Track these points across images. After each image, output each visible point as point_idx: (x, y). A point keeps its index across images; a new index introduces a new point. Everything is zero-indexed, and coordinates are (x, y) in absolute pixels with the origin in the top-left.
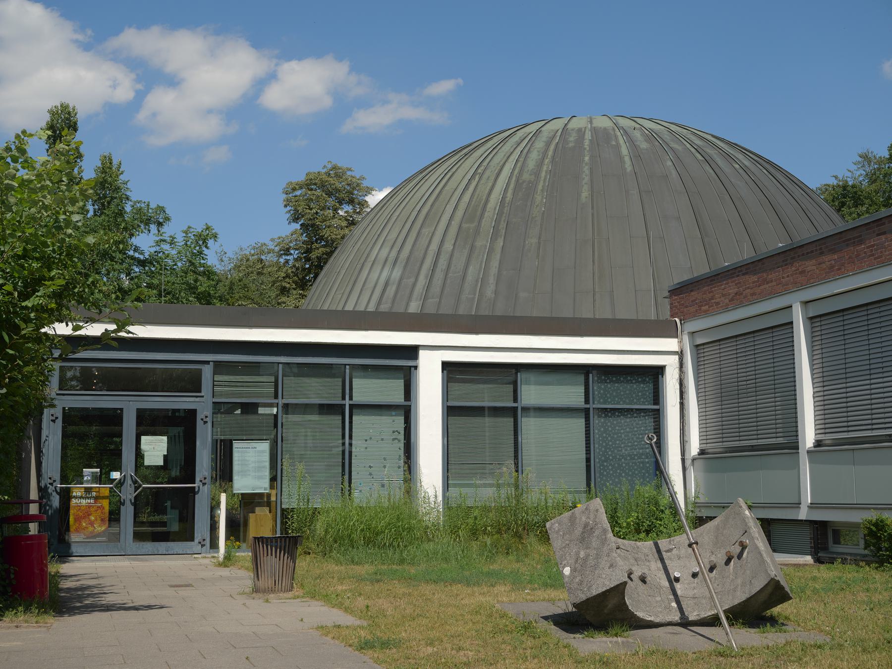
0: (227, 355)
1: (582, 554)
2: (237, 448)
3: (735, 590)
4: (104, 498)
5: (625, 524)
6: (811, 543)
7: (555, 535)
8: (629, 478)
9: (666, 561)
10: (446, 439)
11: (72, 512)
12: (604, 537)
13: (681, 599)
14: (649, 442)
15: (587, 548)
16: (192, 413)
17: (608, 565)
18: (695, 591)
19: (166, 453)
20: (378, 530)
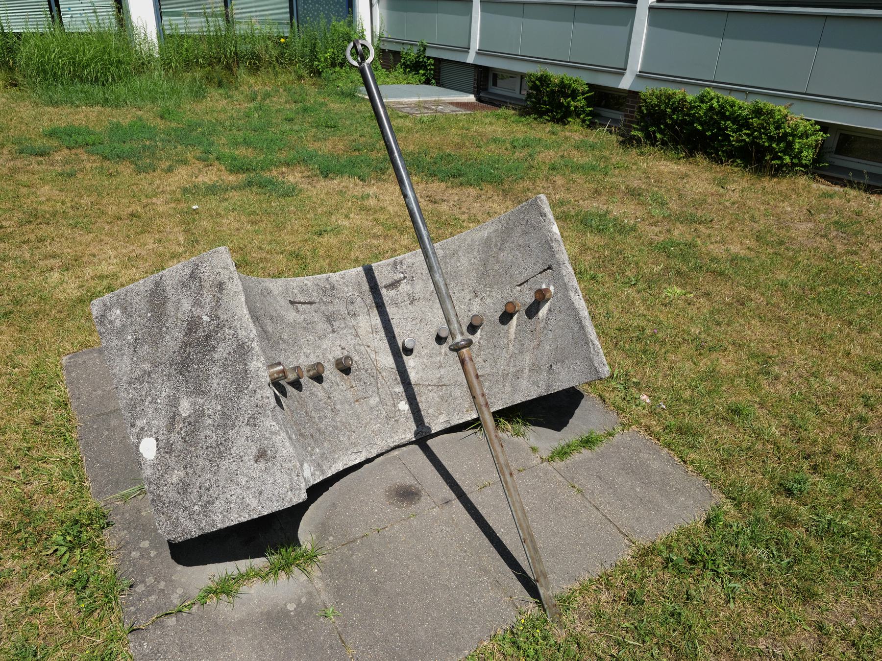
1: (185, 407)
3: (517, 376)
5: (323, 59)
7: (115, 343)
8: (326, 12)
9: (388, 310)
12: (240, 367)
13: (416, 389)
14: (355, 64)
15: (199, 391)
17: (254, 451)
18: (443, 371)
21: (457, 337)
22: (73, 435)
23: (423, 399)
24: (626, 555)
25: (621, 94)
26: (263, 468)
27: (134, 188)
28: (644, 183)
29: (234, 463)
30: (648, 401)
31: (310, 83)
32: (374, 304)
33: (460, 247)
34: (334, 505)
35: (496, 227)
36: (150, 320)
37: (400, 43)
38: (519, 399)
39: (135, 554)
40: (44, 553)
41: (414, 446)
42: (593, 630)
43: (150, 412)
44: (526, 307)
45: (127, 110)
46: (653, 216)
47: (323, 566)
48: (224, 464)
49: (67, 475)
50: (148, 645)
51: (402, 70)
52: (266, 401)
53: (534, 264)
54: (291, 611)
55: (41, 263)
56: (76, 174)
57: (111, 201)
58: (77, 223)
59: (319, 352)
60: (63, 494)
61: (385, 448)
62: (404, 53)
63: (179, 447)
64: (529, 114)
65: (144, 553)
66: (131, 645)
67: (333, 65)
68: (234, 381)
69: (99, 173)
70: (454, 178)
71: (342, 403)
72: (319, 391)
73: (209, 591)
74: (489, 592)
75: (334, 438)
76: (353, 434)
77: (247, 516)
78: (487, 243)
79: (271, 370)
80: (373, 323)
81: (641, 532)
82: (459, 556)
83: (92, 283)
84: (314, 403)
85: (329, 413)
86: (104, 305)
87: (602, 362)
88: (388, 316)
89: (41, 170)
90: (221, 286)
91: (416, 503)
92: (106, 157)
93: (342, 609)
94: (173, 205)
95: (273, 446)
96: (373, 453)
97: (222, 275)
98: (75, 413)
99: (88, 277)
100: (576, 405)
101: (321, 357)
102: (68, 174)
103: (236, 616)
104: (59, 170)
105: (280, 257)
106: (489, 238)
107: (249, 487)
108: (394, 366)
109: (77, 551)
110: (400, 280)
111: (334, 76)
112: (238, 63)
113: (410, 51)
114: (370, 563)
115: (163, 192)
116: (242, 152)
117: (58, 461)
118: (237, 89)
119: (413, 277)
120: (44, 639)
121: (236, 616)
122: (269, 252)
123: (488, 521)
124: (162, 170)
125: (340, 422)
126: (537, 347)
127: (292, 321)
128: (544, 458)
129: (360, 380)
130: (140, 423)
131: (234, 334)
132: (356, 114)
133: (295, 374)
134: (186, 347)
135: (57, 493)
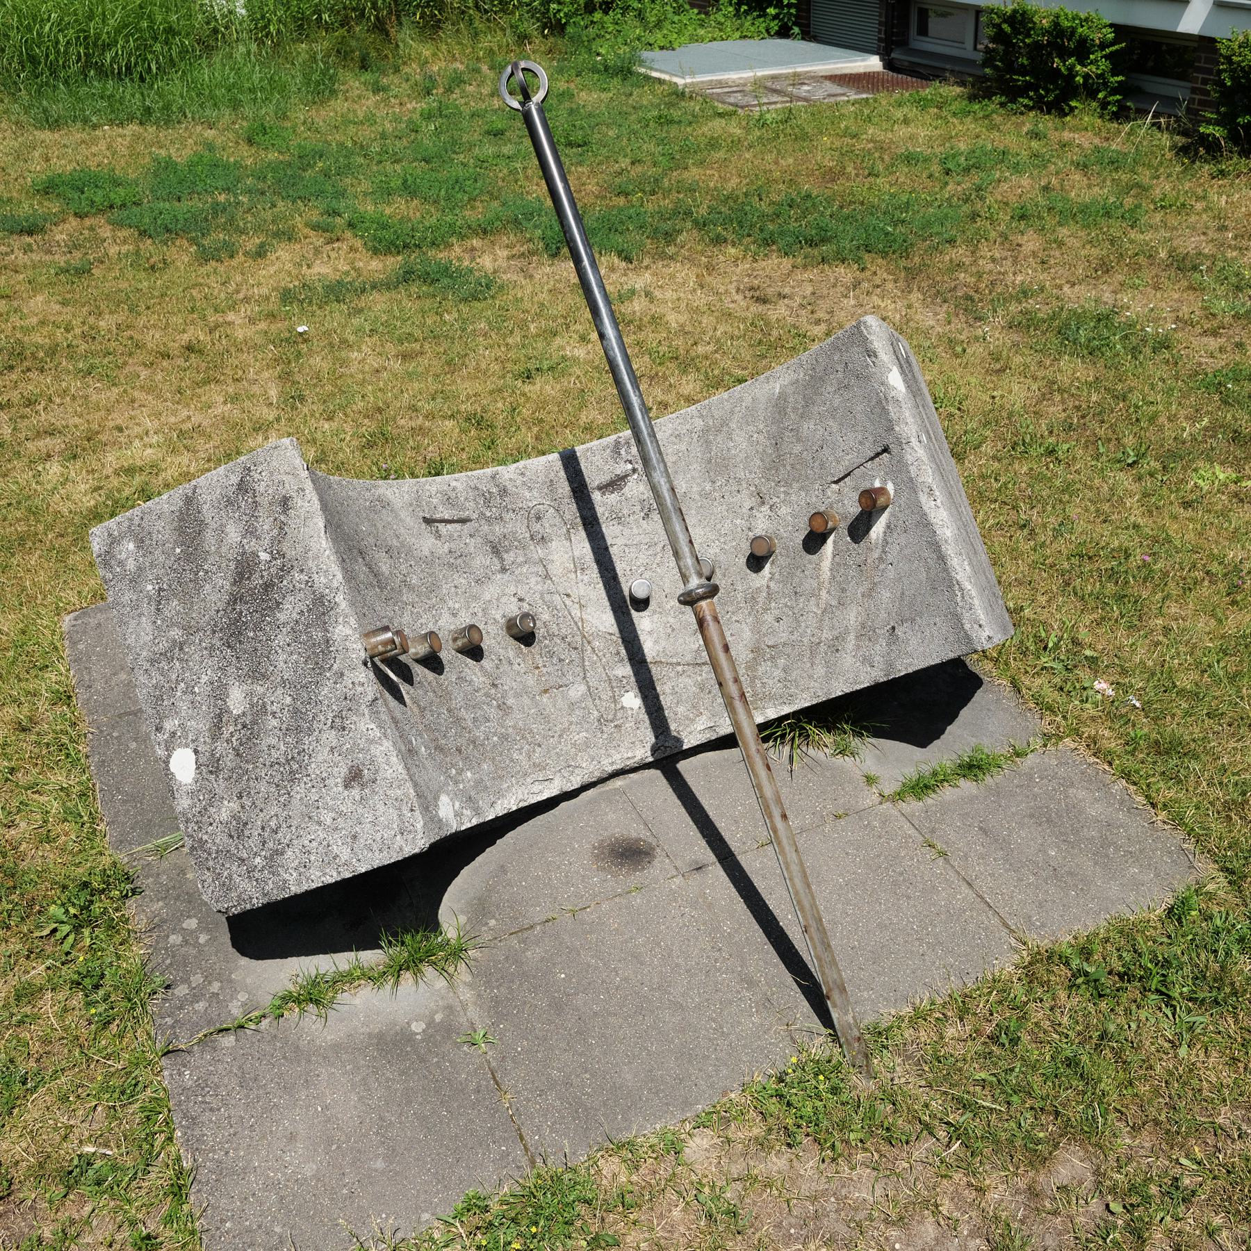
1: (237, 700)
6: (880, 32)
7: (127, 597)
9: (604, 529)
12: (318, 635)
13: (654, 670)
15: (256, 675)
17: (344, 770)
20: (104, 41)
21: (690, 580)
22: (81, 748)
24: (1006, 965)
25: (1187, 43)
26: (358, 798)
27: (194, 292)
28: (1212, 241)
29: (314, 790)
30: (1110, 692)
31: (543, 49)
32: (579, 520)
33: (732, 412)
34: (503, 869)
36: (179, 559)
38: (839, 689)
39: (175, 939)
40: (37, 934)
41: (652, 771)
42: (923, 1083)
43: (183, 706)
44: (849, 521)
45: (186, 128)
46: (1214, 315)
47: (475, 966)
48: (299, 790)
49: (71, 813)
50: (191, 1075)
51: (731, 9)
52: (360, 689)
54: (417, 1034)
55: (29, 445)
56: (91, 269)
57: (152, 322)
58: (92, 367)
59: (476, 607)
60: (66, 843)
61: (597, 774)
63: (229, 764)
64: (988, 95)
65: (189, 938)
66: (166, 1073)
68: (309, 656)
69: (131, 265)
70: (811, 246)
71: (517, 695)
72: (475, 674)
73: (287, 998)
75: (501, 755)
76: (538, 750)
77: (335, 874)
78: (780, 405)
79: (373, 640)
80: (577, 554)
81: (1043, 925)
83: (115, 482)
84: (466, 695)
85: (493, 713)
86: (110, 535)
88: (605, 541)
89: (29, 263)
90: (285, 504)
91: (643, 868)
92: (145, 231)
93: (500, 1034)
94: (263, 325)
95: (372, 762)
96: (574, 783)
97: (287, 485)
98: (84, 712)
99: (109, 471)
100: (965, 699)
101: (480, 614)
102: (76, 269)
103: (328, 1038)
104: (61, 260)
105: (449, 424)
106: (783, 396)
107: (336, 829)
108: (614, 629)
109: (86, 932)
110: (626, 476)
111: (592, 31)
112: (398, 17)
115: (247, 300)
116: (400, 209)
117: (56, 790)
118: (397, 70)
120: (38, 1061)
121: (328, 1038)
122: (430, 416)
123: (767, 902)
124: (246, 254)
125: (514, 727)
126: (869, 594)
127: (427, 553)
128: (886, 795)
129: (551, 654)
130: (169, 725)
131: (308, 582)
132: (630, 114)
133: (427, 645)
134: (235, 602)
135: (55, 842)
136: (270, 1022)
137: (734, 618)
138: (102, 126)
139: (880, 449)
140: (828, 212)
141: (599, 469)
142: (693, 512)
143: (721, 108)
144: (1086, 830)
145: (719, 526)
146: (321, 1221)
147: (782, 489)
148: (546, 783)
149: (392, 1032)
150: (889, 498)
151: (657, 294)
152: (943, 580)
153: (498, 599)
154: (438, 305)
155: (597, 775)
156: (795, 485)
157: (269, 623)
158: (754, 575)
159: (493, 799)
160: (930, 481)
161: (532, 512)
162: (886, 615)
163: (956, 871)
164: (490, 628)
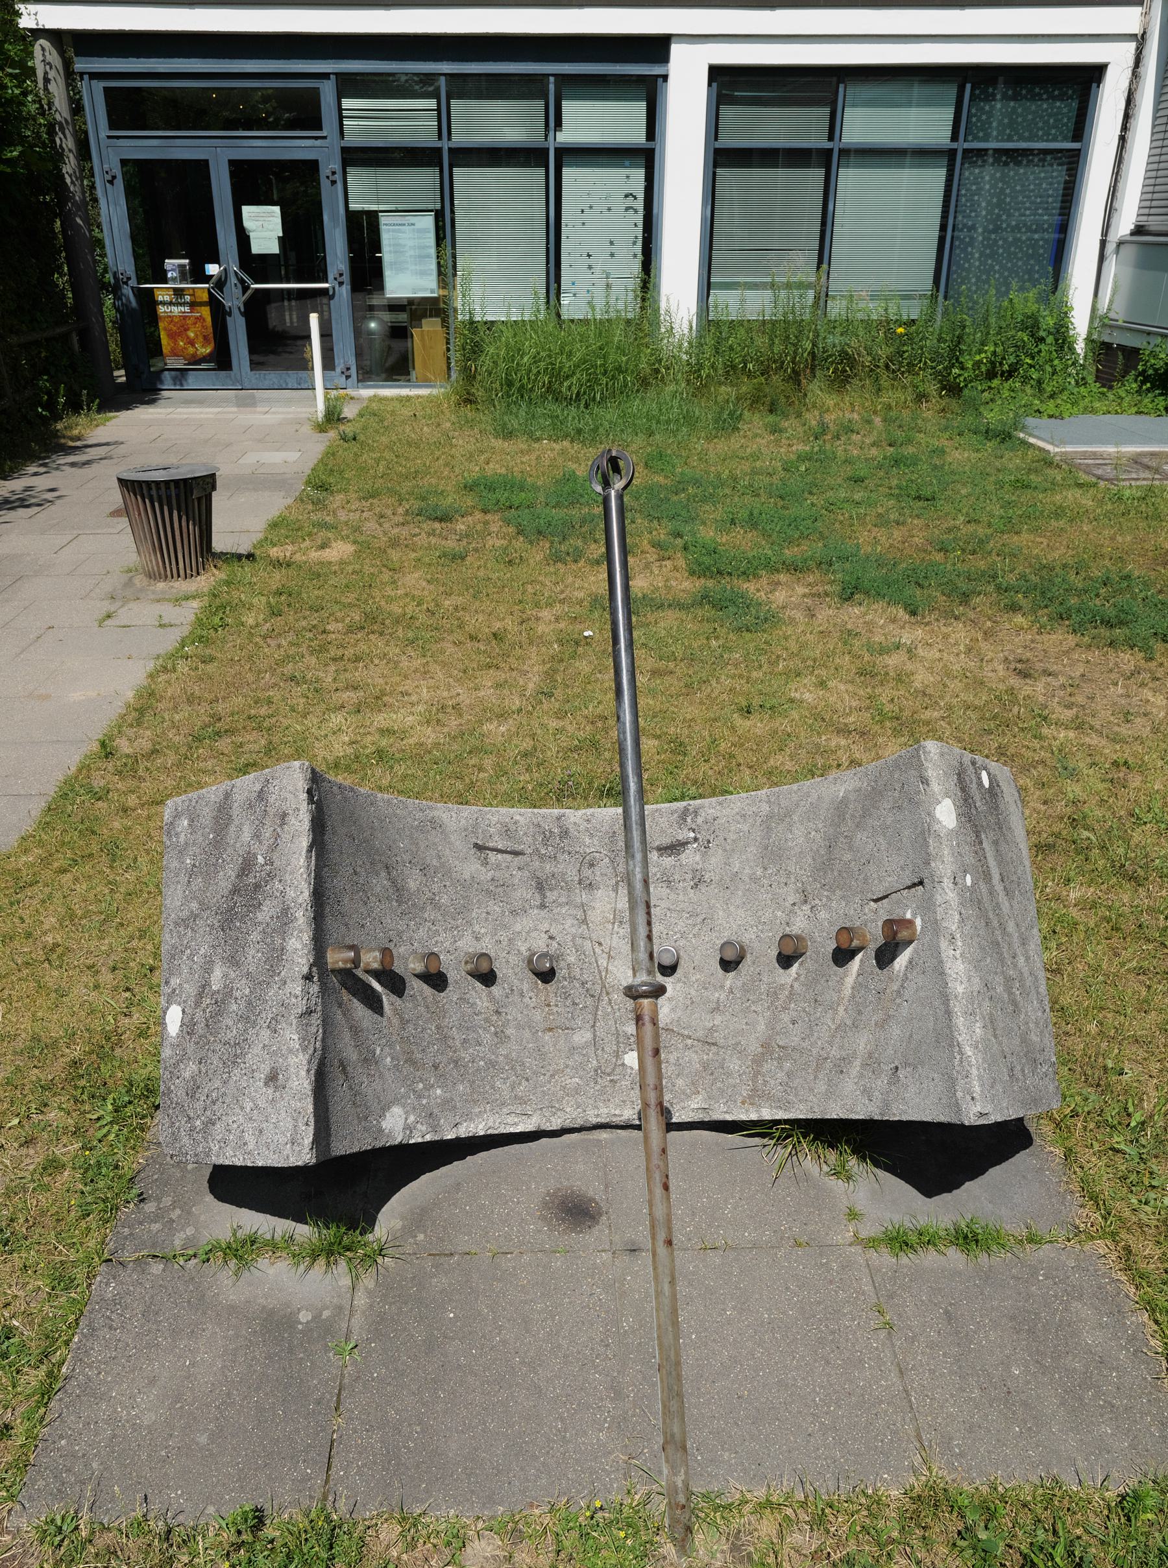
0: (357, 61)
2: (386, 225)
4: (202, 304)
5: (969, 365)
7: (175, 864)
10: (709, 207)
11: (161, 325)
15: (233, 961)
16: (312, 167)
19: (281, 234)
23: (672, 1058)
33: (797, 805)
35: (858, 784)
37: (1143, 332)
38: (835, 1111)
47: (384, 1276)
50: (114, 1288)
53: (902, 869)
54: (301, 1323)
59: (503, 936)
62: (1147, 352)
67: (991, 375)
71: (519, 1027)
72: (480, 998)
74: (601, 1431)
76: (524, 1083)
77: (241, 1158)
78: (841, 808)
82: (592, 1349)
84: (464, 1016)
85: (487, 1038)
87: (970, 1093)
91: (581, 1232)
101: (505, 943)
106: (844, 801)
107: (251, 1119)
113: (1158, 349)
114: (450, 1300)
118: (799, 415)
119: (709, 842)
125: (506, 1057)
126: (882, 1025)
129: (567, 996)
136: (196, 1264)
137: (753, 1008)
138: (543, 439)
139: (916, 880)
140: (1142, 595)
141: (663, 831)
142: (740, 893)
143: (1083, 477)
144: (1070, 1358)
145: (760, 913)
146: (130, 1474)
147: (825, 893)
148: (524, 1117)
149: (282, 1313)
150: (914, 933)
151: (920, 652)
152: (946, 1038)
153: (528, 932)
154: (712, 630)
155: (579, 1123)
156: (838, 893)
157: (251, 919)
158: (782, 971)
159: (458, 1121)
160: (954, 928)
161: (587, 858)
162: (892, 1052)
163: (894, 1351)
164: (511, 958)
